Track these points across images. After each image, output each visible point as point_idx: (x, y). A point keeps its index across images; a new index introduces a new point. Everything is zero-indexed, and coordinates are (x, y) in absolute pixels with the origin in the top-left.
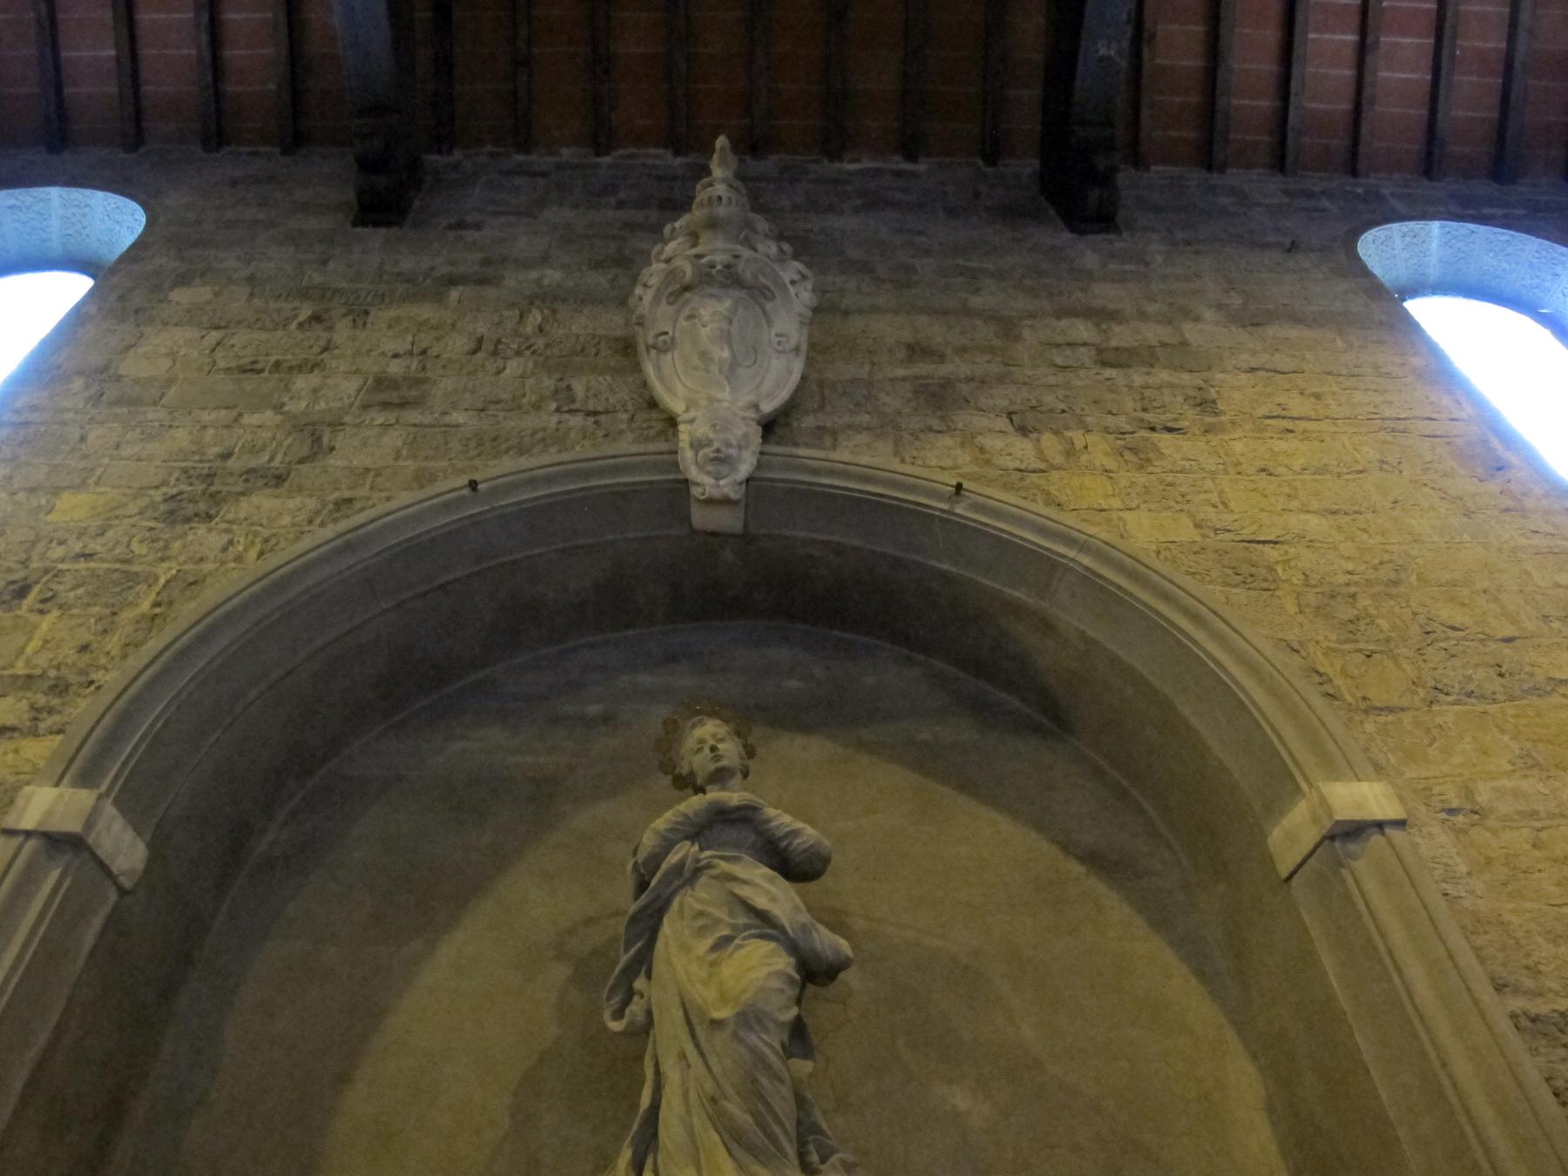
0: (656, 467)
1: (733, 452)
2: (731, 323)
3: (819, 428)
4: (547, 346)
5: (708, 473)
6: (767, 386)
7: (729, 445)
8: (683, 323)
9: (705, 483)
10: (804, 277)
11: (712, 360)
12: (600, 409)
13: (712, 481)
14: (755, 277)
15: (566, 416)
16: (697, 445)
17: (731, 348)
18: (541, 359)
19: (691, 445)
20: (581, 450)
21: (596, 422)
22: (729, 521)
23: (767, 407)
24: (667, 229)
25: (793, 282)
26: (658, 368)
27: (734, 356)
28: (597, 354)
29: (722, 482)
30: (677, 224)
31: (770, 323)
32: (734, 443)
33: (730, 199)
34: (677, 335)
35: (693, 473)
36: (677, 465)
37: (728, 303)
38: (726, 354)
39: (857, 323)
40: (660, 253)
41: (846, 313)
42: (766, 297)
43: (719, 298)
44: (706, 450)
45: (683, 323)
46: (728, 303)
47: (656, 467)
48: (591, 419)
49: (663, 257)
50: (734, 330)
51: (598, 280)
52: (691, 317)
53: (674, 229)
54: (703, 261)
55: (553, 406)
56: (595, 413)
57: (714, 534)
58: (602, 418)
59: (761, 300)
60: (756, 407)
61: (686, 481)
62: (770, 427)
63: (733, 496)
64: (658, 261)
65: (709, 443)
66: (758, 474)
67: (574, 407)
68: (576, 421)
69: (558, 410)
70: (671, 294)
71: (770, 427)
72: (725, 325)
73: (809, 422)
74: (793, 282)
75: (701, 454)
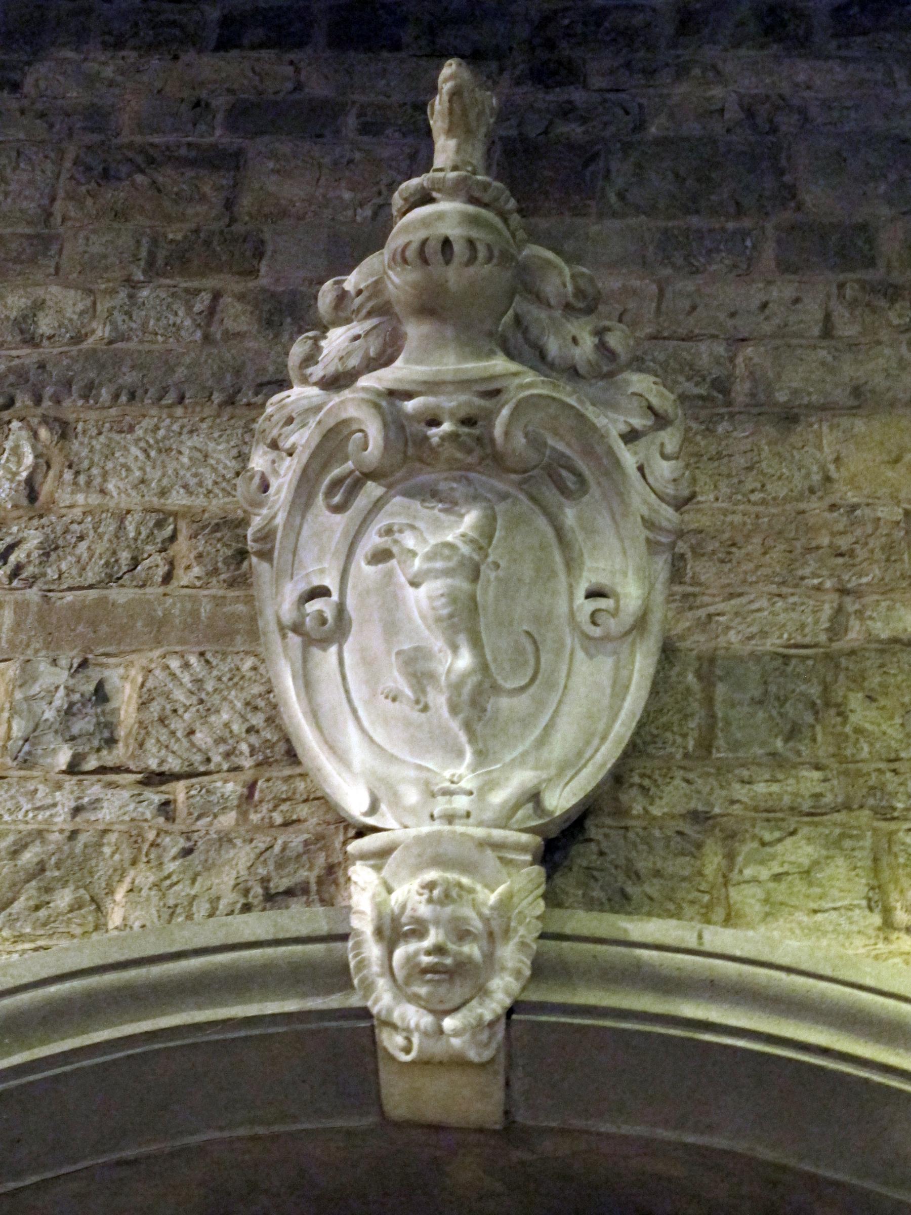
0: (299, 977)
1: (472, 950)
2: (475, 575)
3: (695, 817)
4: (49, 550)
5: (415, 999)
6: (560, 745)
7: (463, 934)
8: (365, 571)
9: (406, 1023)
10: (661, 421)
11: (431, 676)
12: (174, 764)
13: (427, 1020)
14: (536, 442)
15: (94, 789)
16: (392, 932)
17: (476, 644)
18: (33, 594)
19: (379, 932)
20: (130, 920)
21: (166, 808)
22: (475, 1103)
23: (561, 800)
24: (326, 294)
25: (631, 436)
26: (307, 683)
27: (483, 667)
28: (168, 578)
29: (449, 1023)
30: (351, 282)
31: (572, 564)
32: (477, 925)
33: (471, 243)
34: (351, 603)
35: (381, 998)
36: (344, 968)
37: (471, 518)
38: (464, 661)
39: (824, 443)
40: (310, 359)
41: (789, 418)
42: (564, 490)
43: (452, 505)
44: (412, 946)
45: (365, 571)
46: (471, 518)
47: (299, 977)
48: (154, 797)
49: (317, 372)
50: (487, 595)
51: (165, 317)
52: (381, 556)
53: (342, 296)
54: (410, 406)
55: (63, 757)
56: (156, 778)
57: (436, 1128)
58: (179, 790)
59: (551, 494)
60: (534, 797)
61: (365, 1013)
62: (561, 845)
63: (473, 1055)
64: (305, 380)
65: (419, 930)
66: (534, 996)
67: (109, 758)
68: (116, 805)
69: (73, 769)
70: (336, 484)
71: (561, 845)
72: (462, 584)
73: (671, 799)
74: (631, 436)
75: (399, 954)
